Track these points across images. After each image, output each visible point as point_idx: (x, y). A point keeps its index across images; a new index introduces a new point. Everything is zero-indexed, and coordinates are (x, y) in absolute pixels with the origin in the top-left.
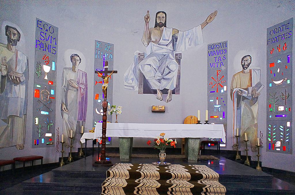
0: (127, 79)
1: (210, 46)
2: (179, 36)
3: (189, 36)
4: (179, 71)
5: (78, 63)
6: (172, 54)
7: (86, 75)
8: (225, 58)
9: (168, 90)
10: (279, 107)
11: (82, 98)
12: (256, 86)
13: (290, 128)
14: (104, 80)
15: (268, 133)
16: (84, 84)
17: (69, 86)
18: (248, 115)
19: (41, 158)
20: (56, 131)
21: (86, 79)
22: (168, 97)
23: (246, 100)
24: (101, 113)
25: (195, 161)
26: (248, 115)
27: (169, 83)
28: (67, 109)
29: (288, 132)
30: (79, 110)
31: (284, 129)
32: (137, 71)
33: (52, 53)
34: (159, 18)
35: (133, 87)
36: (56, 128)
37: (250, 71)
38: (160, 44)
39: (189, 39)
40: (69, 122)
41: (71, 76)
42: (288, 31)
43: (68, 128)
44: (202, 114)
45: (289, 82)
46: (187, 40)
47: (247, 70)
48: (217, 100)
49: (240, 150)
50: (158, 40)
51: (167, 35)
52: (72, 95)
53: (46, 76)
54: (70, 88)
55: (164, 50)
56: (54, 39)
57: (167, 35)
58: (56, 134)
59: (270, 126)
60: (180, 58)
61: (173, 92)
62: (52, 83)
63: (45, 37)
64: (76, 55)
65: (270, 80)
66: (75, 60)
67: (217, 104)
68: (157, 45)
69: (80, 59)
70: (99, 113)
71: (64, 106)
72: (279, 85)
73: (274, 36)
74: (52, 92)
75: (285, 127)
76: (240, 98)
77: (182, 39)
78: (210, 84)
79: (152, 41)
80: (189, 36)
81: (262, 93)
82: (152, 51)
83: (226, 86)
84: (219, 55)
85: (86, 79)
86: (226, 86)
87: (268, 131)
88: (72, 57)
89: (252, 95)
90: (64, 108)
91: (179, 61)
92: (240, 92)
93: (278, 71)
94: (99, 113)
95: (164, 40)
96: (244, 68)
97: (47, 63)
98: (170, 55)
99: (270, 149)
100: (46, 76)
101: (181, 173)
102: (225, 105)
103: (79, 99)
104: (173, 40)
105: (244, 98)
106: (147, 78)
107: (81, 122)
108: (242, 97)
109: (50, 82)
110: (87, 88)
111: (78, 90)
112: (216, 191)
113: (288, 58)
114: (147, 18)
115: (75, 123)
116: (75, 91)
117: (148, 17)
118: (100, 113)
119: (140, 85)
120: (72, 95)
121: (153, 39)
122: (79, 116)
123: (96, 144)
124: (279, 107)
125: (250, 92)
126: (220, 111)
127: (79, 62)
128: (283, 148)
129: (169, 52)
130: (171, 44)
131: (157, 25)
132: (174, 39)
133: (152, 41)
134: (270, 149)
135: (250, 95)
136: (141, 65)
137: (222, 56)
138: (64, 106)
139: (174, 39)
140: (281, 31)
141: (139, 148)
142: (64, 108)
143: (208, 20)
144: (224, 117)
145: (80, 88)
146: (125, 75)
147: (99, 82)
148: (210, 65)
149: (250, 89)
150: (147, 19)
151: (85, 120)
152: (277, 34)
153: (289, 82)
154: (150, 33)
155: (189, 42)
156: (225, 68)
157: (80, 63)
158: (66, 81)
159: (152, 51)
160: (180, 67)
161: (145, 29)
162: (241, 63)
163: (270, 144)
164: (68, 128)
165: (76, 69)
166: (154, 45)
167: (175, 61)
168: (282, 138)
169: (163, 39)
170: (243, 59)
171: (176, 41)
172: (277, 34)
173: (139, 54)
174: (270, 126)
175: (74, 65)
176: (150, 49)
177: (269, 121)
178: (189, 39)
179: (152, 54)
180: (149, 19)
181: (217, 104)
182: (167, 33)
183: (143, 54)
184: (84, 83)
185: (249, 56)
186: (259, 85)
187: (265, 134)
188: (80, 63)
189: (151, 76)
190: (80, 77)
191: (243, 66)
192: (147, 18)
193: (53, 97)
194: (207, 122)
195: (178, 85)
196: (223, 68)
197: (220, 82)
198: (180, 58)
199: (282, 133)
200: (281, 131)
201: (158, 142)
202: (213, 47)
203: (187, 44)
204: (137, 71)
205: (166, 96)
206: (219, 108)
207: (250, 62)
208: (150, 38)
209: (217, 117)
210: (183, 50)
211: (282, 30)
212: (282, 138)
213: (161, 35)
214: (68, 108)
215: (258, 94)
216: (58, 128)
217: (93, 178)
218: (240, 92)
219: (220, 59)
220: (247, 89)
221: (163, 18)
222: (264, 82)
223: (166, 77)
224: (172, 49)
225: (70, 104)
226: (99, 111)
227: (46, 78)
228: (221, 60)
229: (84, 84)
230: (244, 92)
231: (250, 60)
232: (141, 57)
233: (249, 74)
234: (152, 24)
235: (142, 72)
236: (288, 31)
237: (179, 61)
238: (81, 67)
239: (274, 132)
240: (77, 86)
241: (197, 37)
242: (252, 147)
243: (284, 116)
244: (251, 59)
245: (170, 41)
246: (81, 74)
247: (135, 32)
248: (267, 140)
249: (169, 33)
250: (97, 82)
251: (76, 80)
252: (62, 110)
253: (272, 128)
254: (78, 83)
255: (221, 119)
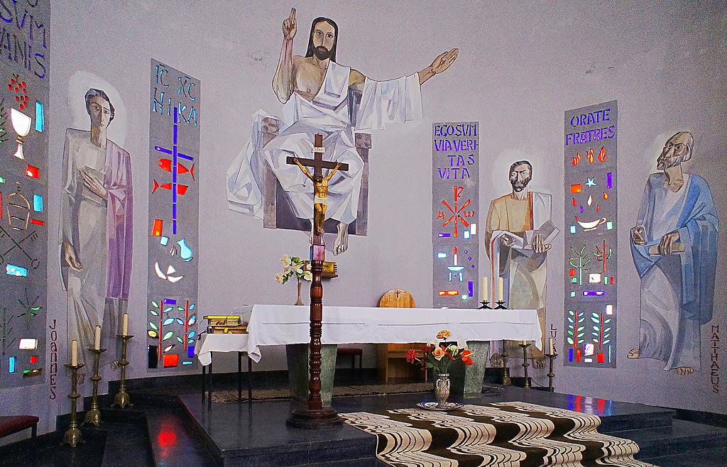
0: (234, 184)
1: (439, 127)
2: (366, 89)
3: (390, 95)
4: (365, 177)
5: (105, 118)
6: (349, 133)
7: (128, 158)
8: (473, 160)
9: (339, 222)
10: (591, 275)
11: (119, 229)
12: (543, 228)
13: (613, 318)
14: (319, 184)
15: (567, 329)
16: (123, 187)
17: (81, 190)
18: (524, 291)
19: (32, 422)
20: (49, 332)
21: (128, 172)
22: (338, 242)
23: (519, 258)
24: (171, 275)
25: (476, 394)
26: (524, 291)
27: (339, 206)
28: (78, 260)
29: (608, 325)
30: (110, 267)
31: (602, 319)
32: (261, 164)
33: (36, 73)
34: (320, 33)
35: (251, 208)
36: (50, 322)
37: (530, 195)
38: (320, 103)
39: (389, 104)
40: (84, 301)
41: (88, 157)
42: (608, 124)
43: (81, 318)
44: (423, 286)
45: (610, 226)
46: (385, 104)
47: (522, 194)
48: (456, 256)
49: (507, 366)
50: (313, 92)
51: (336, 82)
52: (91, 218)
53: (20, 148)
54: (86, 194)
55: (325, 121)
56: (39, 27)
57: (336, 82)
58: (49, 342)
59: (572, 313)
60: (366, 145)
61: (351, 229)
62: (36, 171)
63: (14, 13)
64: (102, 93)
65: (572, 219)
66: (99, 108)
67: (456, 264)
68: (311, 104)
69: (112, 110)
70: (164, 277)
71: (70, 252)
72: (591, 233)
73: (581, 129)
74: (37, 205)
75: (603, 317)
76: (506, 253)
77: (373, 100)
78: (438, 215)
79: (298, 92)
80: (390, 95)
81: (556, 245)
82: (298, 118)
83: (475, 225)
84: (460, 152)
85: (128, 172)
86: (475, 225)
87: (567, 323)
88: (90, 97)
89: (534, 248)
90: (71, 258)
91: (364, 152)
92: (507, 239)
93: (590, 202)
94: (164, 277)
95: (329, 94)
96: (515, 188)
97: (21, 102)
98: (343, 134)
99: (571, 360)
100: (20, 148)
101: (477, 428)
102: (473, 266)
103: (110, 233)
104: (350, 96)
105: (516, 254)
106: (285, 187)
107: (116, 300)
108: (511, 251)
109: (30, 168)
110: (130, 200)
111: (106, 201)
112: (624, 452)
113: (609, 176)
114: (289, 28)
115: (101, 305)
116: (98, 205)
117: (292, 26)
118: (166, 275)
119: (267, 205)
120: (91, 218)
121: (301, 87)
122: (111, 286)
123: (111, 383)
124: (591, 275)
125: (529, 241)
126: (461, 280)
127: (109, 116)
128: (599, 358)
129: (340, 127)
130: (346, 108)
131: (312, 51)
132: (354, 97)
133: (298, 92)
134: (571, 360)
135: (529, 247)
136: (271, 152)
137: (465, 155)
138: (70, 252)
139: (354, 97)
140: (594, 122)
141: (269, 372)
142: (71, 258)
143: (436, 66)
144: (471, 295)
145: (113, 197)
146: (231, 172)
147: (161, 186)
148: (439, 173)
149: (530, 235)
150: (289, 29)
151: (125, 295)
152: (587, 127)
153: (610, 226)
154: (294, 70)
155: (390, 110)
156: (473, 184)
157: (111, 119)
158: (73, 173)
159: (298, 118)
160: (366, 168)
161: (283, 54)
162: (510, 177)
163: (571, 350)
164: (81, 318)
165: (102, 137)
166: (302, 102)
167: (354, 150)
168: (596, 337)
169: (325, 91)
170: (512, 169)
171: (358, 102)
172: (587, 127)
173: (266, 120)
174: (572, 313)
175: (96, 123)
176: (293, 111)
177: (569, 303)
178: (390, 101)
179: (297, 126)
180: (293, 31)
181: (456, 264)
182: (337, 78)
183: (274, 122)
184: (124, 183)
185: (528, 163)
186: (548, 228)
187: (561, 333)
188: (111, 119)
189: (297, 182)
190: (111, 163)
191: (513, 183)
192: (289, 28)
193: (39, 221)
194: (501, 306)
195: (363, 213)
196: (468, 182)
197: (461, 214)
198: (366, 145)
199: (596, 328)
200: (596, 324)
201: (440, 354)
202: (444, 131)
203: (385, 115)
204: (261, 164)
205: (333, 239)
206: (460, 274)
207: (528, 176)
208: (293, 81)
209: (456, 292)
210: (375, 127)
211: (596, 120)
212: (596, 337)
213: (322, 80)
214: (81, 257)
215: (547, 246)
216: (55, 321)
217: (341, 458)
218: (507, 239)
219: (461, 160)
220: (522, 234)
221: (329, 36)
222: (560, 222)
223: (332, 189)
224: (347, 121)
225: (86, 246)
226: (164, 271)
227: (19, 154)
228: (464, 164)
229: (123, 187)
230: (517, 242)
231: (528, 171)
232: (270, 130)
233: (527, 201)
234: (301, 48)
235: (274, 169)
236: (608, 124)
237: (364, 152)
238: (114, 132)
239: (581, 325)
240: (103, 192)
241: (407, 100)
242: (533, 359)
243: (599, 293)
244: (531, 169)
245: (343, 98)
246: (115, 156)
247: (256, 59)
248: (566, 341)
249: (341, 79)
250: (157, 185)
251: (102, 172)
252: (64, 264)
253: (576, 319)
254: (108, 183)
255: (465, 297)
